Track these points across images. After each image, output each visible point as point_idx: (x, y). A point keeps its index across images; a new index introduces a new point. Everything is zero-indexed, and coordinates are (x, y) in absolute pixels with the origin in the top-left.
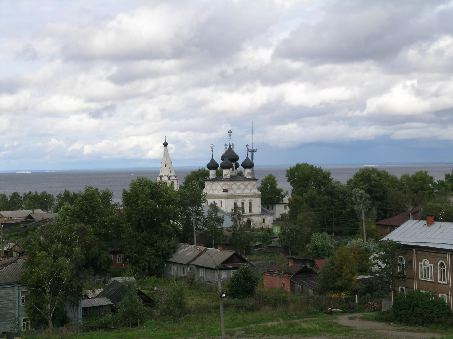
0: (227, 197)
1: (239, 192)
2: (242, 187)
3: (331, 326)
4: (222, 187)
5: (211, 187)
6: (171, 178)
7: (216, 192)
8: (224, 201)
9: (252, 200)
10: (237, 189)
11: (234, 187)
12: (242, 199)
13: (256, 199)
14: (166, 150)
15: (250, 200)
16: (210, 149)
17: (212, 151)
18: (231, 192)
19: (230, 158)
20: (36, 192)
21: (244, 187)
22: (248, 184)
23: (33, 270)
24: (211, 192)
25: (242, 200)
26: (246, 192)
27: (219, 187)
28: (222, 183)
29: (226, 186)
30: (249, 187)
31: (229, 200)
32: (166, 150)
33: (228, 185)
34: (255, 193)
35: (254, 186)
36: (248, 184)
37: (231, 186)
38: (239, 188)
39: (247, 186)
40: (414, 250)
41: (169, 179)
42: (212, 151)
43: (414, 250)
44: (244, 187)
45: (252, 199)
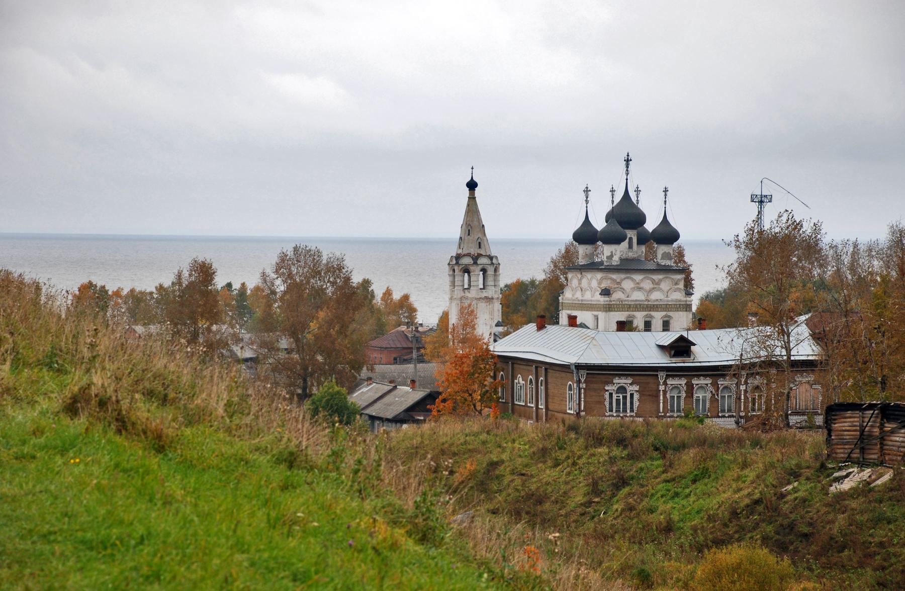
0: (609, 308)
1: (638, 296)
2: (647, 285)
3: (504, 557)
4: (600, 283)
5: (580, 284)
6: (479, 262)
7: (588, 296)
8: (601, 315)
9: (669, 317)
10: (633, 289)
11: (627, 285)
12: (644, 313)
13: (681, 313)
14: (472, 198)
15: (666, 316)
16: (583, 195)
17: (587, 202)
18: (617, 296)
19: (626, 216)
20: (243, 284)
21: (652, 286)
22: (660, 280)
23: (557, 535)
24: (578, 295)
25: (646, 316)
26: (656, 296)
27: (594, 284)
28: (599, 275)
29: (609, 282)
30: (665, 286)
31: (612, 313)
32: (472, 198)
33: (613, 280)
34: (677, 300)
35: (676, 284)
36: (660, 280)
37: (619, 283)
38: (640, 289)
39: (658, 284)
40: (662, 375)
41: (475, 263)
42: (587, 202)
43: (662, 375)
44: (652, 286)
45: (653, 313)
